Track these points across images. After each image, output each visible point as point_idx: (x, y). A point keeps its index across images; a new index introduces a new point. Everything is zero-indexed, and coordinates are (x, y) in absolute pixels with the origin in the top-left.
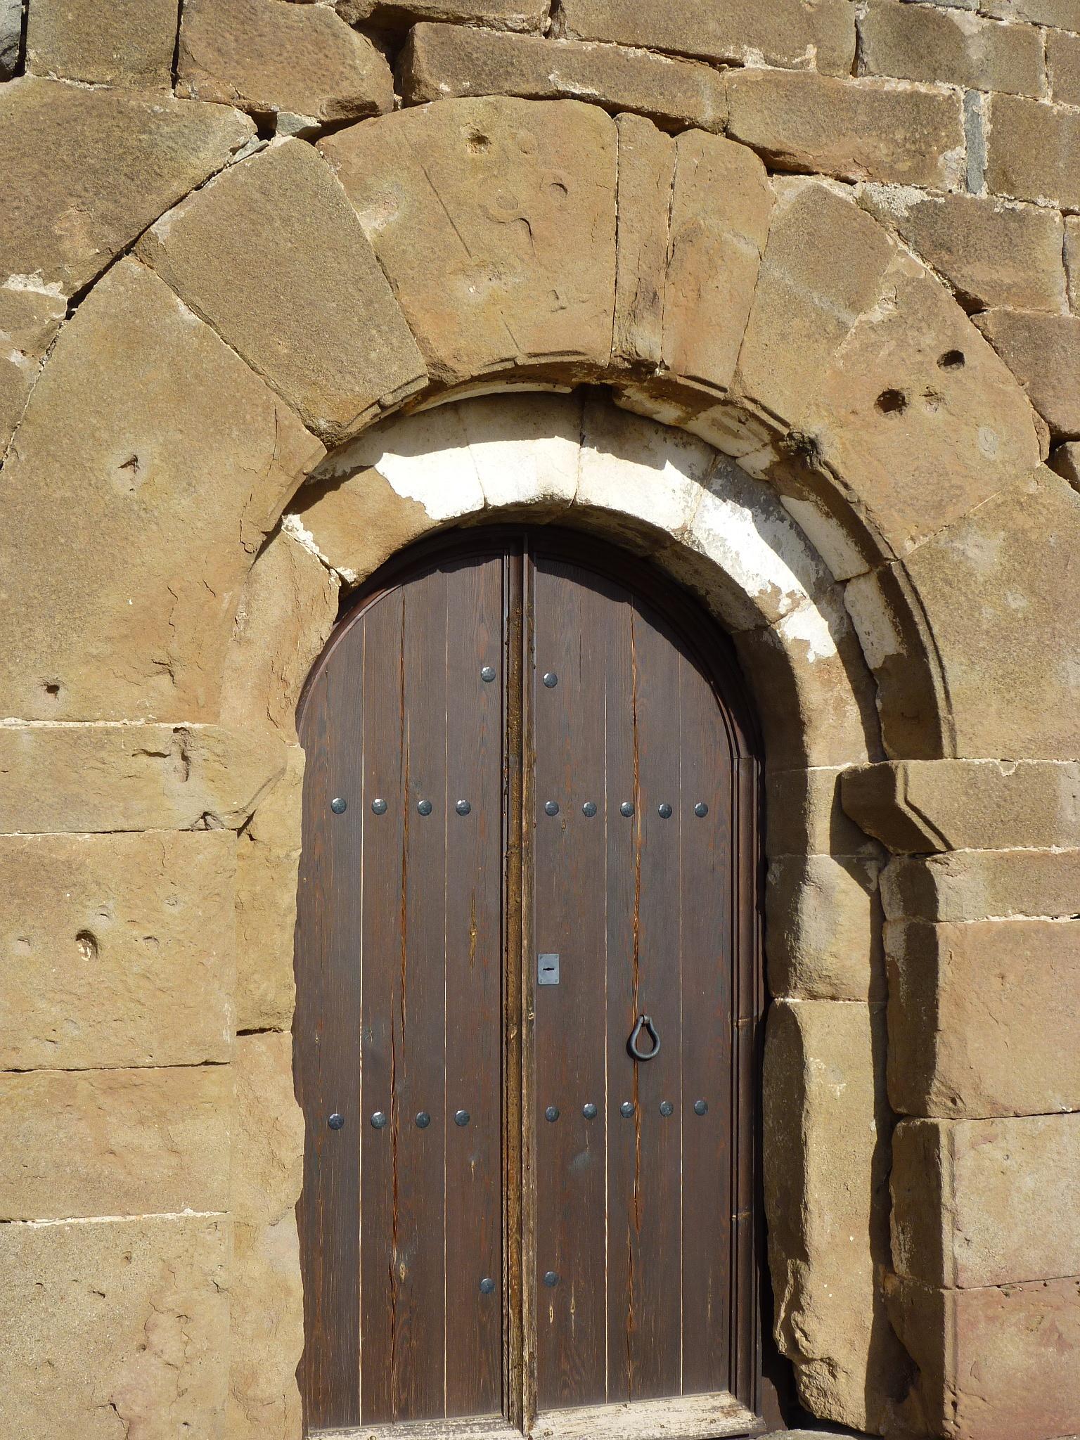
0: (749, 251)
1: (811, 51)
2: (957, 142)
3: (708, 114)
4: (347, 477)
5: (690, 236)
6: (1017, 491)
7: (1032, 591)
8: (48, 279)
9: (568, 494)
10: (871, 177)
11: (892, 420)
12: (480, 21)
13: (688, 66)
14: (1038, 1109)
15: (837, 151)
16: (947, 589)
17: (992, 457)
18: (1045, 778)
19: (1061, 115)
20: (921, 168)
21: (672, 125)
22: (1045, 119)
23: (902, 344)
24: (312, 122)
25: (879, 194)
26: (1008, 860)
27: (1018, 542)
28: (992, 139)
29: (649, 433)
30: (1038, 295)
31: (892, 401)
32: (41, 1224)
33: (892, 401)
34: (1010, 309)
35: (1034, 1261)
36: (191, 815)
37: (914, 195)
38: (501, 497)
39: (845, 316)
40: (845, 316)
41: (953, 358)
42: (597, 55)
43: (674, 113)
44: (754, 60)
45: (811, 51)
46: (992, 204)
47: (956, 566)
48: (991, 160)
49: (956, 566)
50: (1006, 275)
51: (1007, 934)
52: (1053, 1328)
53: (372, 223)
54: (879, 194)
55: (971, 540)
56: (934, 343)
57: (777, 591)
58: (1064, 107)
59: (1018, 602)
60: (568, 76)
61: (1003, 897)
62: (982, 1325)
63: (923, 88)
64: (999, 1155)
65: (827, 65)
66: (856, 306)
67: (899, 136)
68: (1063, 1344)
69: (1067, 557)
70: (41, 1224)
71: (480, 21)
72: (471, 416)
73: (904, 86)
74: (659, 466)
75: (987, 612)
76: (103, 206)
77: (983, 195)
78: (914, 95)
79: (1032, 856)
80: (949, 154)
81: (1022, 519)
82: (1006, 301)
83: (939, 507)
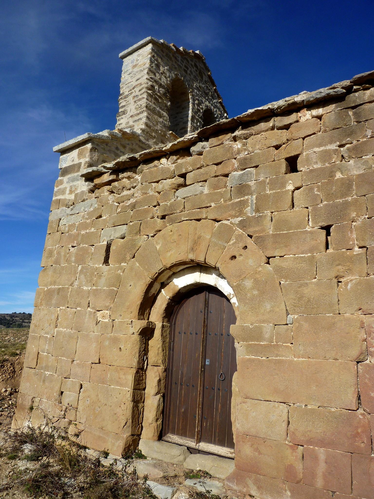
0: (208, 237)
1: (222, 199)
2: (248, 206)
3: (204, 216)
4: (169, 283)
5: (199, 237)
6: (256, 271)
7: (258, 290)
8: (125, 263)
9: (198, 281)
10: (232, 218)
11: (233, 262)
12: (174, 213)
13: (201, 209)
14: (255, 398)
15: (225, 216)
16: (241, 291)
17: (251, 265)
18: (260, 328)
19: (271, 194)
20: (241, 213)
21: (199, 220)
22: (267, 196)
23: (235, 247)
24: (152, 235)
25: (233, 220)
26: (251, 345)
27: (256, 281)
28: (256, 203)
29: (211, 269)
30: (263, 230)
31: (234, 257)
32: (112, 387)
33: (234, 257)
34: (257, 235)
35: (253, 431)
36: (132, 332)
37: (240, 219)
38: (189, 283)
39: (226, 245)
40: (226, 245)
41: (246, 247)
42: (189, 213)
43: (199, 218)
44: (213, 205)
45: (222, 199)
46: (255, 216)
47: (243, 287)
48: (255, 208)
49: (243, 287)
50: (257, 229)
51: (249, 360)
52: (257, 449)
53: (158, 247)
54: (233, 220)
55: (246, 282)
56: (241, 245)
57: (230, 294)
58: (271, 192)
59: (256, 292)
60: (184, 218)
61: (248, 353)
62: (241, 442)
63: (242, 199)
64: (246, 406)
65: (225, 201)
66: (228, 242)
67: (237, 209)
68: (260, 453)
69: (267, 282)
70: (112, 387)
71: (174, 213)
72: (186, 271)
73: (239, 199)
74: (212, 274)
75: (249, 295)
76: (130, 252)
77: (254, 214)
78: (241, 200)
79: (256, 344)
80: (246, 209)
81: (257, 276)
82: (257, 234)
83: (240, 276)
